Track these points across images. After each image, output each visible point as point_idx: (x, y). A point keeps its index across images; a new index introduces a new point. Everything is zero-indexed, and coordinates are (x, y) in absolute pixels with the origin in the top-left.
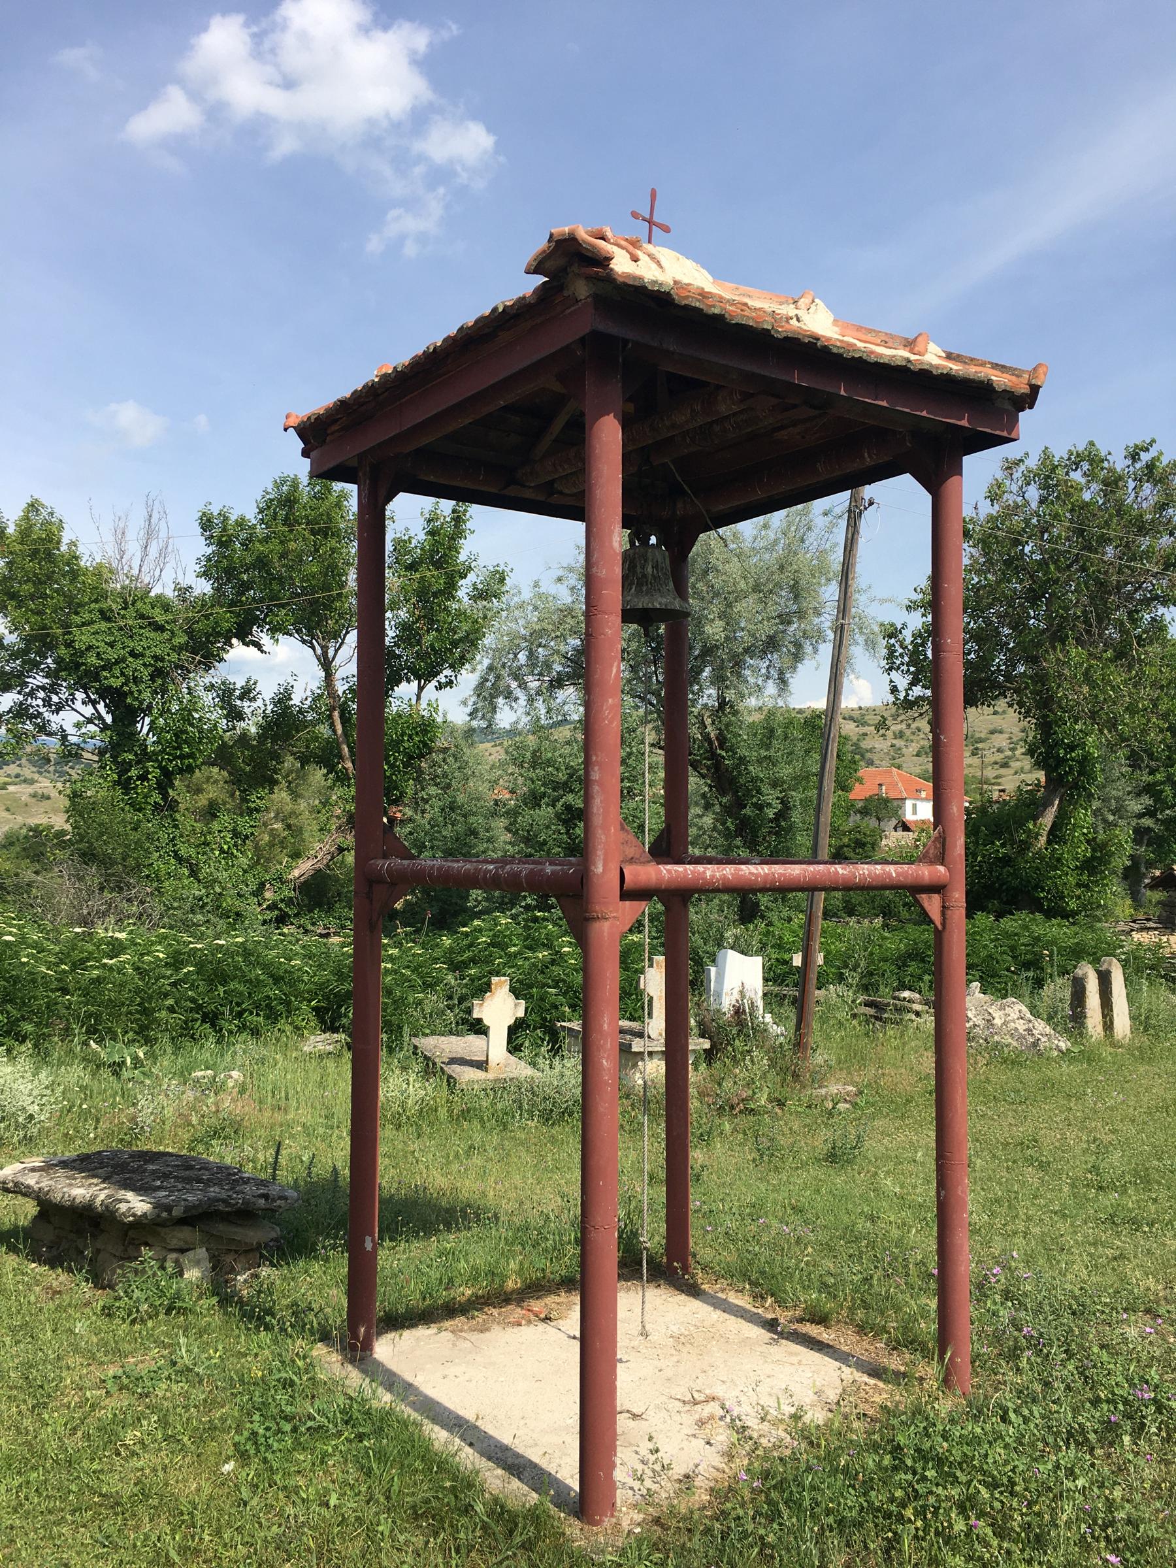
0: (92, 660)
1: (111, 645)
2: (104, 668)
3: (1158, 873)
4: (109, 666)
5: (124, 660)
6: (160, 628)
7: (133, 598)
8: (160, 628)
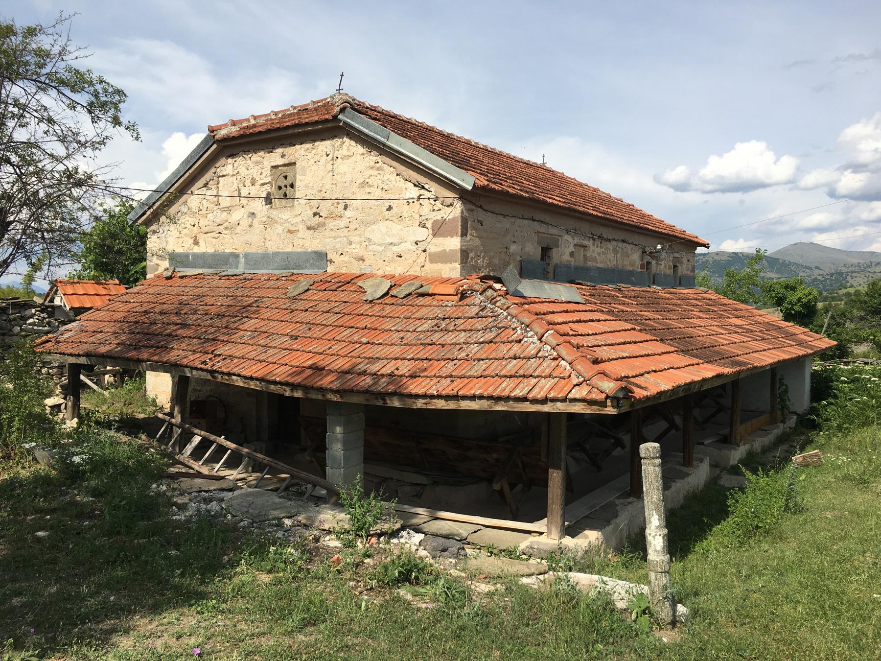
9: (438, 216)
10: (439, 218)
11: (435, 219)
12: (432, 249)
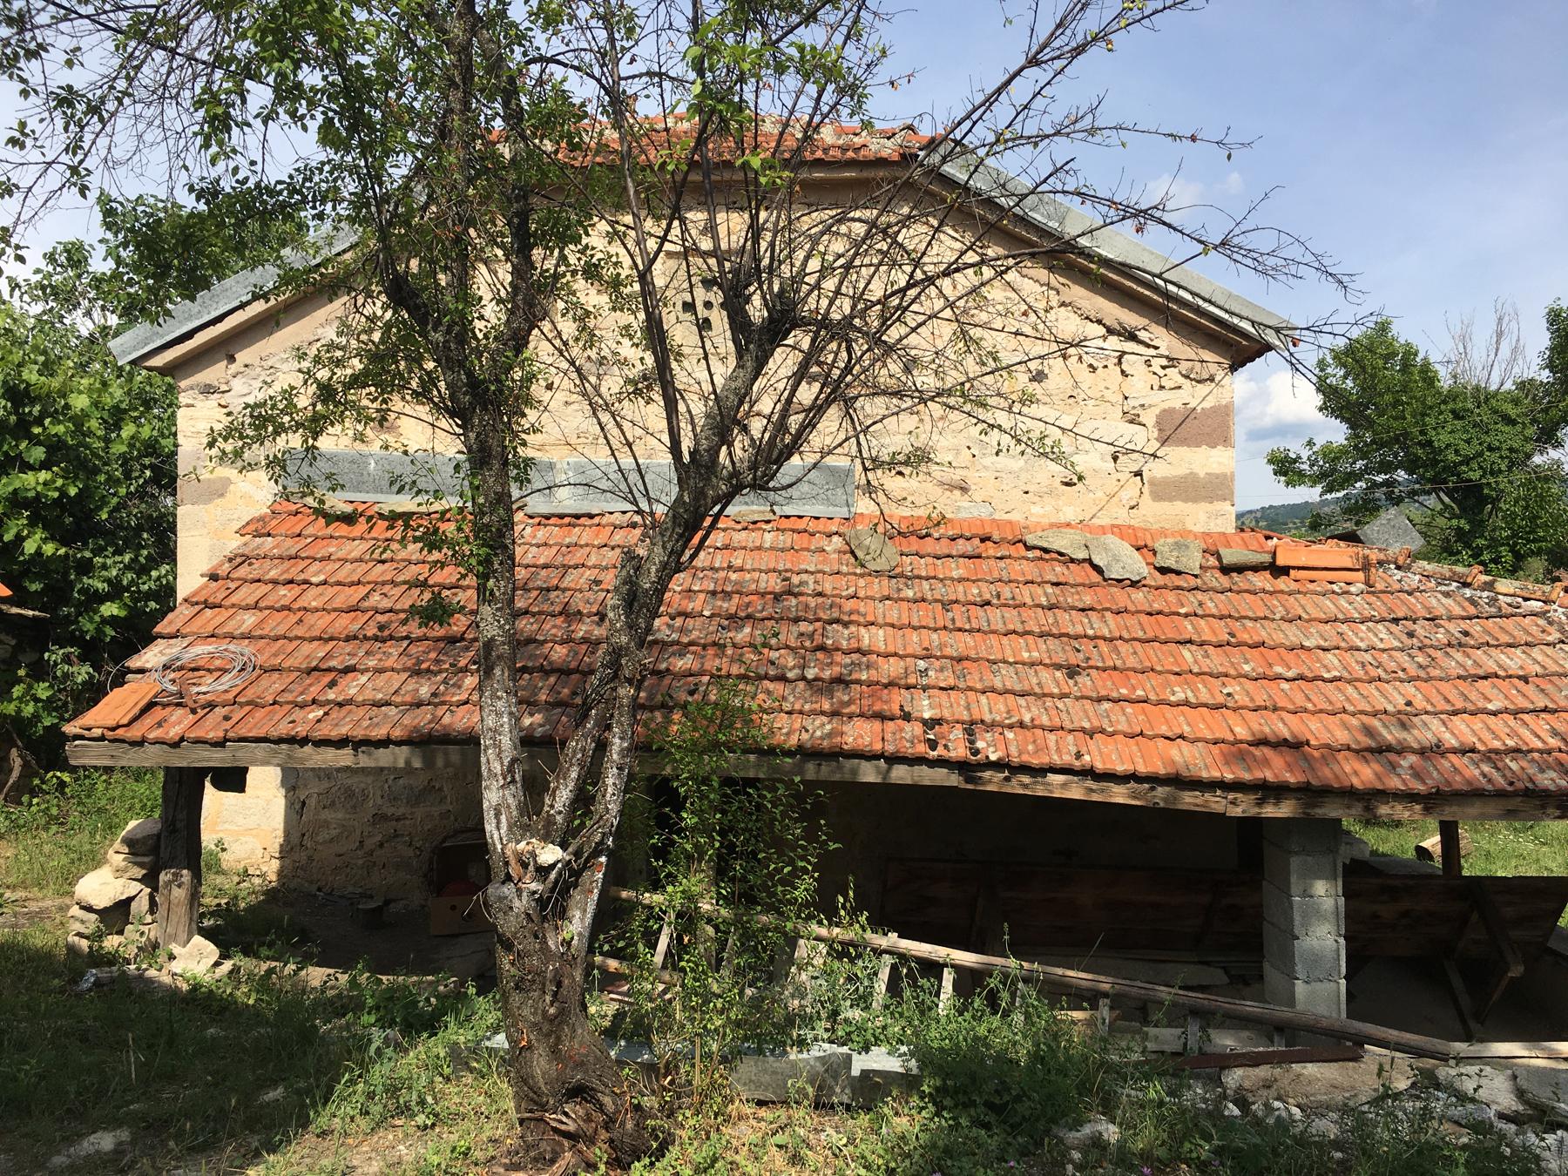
0: (1452, 457)
1: (1468, 442)
2: (1461, 463)
3: (310, 39)
4: (1467, 461)
5: (1481, 454)
6: (1511, 422)
7: (1483, 397)
8: (1511, 422)
9: (1175, 401)
10: (1178, 405)
11: (1166, 406)
12: (1155, 470)
